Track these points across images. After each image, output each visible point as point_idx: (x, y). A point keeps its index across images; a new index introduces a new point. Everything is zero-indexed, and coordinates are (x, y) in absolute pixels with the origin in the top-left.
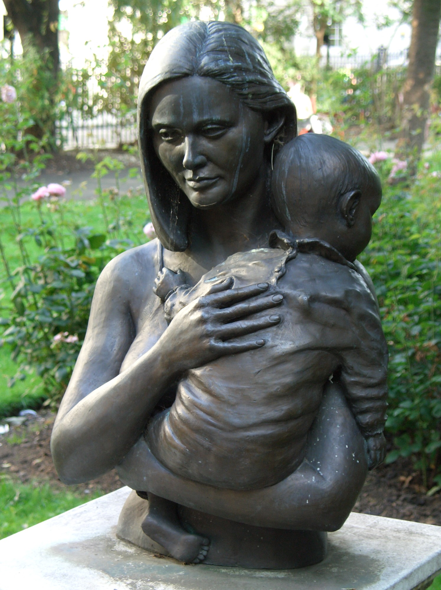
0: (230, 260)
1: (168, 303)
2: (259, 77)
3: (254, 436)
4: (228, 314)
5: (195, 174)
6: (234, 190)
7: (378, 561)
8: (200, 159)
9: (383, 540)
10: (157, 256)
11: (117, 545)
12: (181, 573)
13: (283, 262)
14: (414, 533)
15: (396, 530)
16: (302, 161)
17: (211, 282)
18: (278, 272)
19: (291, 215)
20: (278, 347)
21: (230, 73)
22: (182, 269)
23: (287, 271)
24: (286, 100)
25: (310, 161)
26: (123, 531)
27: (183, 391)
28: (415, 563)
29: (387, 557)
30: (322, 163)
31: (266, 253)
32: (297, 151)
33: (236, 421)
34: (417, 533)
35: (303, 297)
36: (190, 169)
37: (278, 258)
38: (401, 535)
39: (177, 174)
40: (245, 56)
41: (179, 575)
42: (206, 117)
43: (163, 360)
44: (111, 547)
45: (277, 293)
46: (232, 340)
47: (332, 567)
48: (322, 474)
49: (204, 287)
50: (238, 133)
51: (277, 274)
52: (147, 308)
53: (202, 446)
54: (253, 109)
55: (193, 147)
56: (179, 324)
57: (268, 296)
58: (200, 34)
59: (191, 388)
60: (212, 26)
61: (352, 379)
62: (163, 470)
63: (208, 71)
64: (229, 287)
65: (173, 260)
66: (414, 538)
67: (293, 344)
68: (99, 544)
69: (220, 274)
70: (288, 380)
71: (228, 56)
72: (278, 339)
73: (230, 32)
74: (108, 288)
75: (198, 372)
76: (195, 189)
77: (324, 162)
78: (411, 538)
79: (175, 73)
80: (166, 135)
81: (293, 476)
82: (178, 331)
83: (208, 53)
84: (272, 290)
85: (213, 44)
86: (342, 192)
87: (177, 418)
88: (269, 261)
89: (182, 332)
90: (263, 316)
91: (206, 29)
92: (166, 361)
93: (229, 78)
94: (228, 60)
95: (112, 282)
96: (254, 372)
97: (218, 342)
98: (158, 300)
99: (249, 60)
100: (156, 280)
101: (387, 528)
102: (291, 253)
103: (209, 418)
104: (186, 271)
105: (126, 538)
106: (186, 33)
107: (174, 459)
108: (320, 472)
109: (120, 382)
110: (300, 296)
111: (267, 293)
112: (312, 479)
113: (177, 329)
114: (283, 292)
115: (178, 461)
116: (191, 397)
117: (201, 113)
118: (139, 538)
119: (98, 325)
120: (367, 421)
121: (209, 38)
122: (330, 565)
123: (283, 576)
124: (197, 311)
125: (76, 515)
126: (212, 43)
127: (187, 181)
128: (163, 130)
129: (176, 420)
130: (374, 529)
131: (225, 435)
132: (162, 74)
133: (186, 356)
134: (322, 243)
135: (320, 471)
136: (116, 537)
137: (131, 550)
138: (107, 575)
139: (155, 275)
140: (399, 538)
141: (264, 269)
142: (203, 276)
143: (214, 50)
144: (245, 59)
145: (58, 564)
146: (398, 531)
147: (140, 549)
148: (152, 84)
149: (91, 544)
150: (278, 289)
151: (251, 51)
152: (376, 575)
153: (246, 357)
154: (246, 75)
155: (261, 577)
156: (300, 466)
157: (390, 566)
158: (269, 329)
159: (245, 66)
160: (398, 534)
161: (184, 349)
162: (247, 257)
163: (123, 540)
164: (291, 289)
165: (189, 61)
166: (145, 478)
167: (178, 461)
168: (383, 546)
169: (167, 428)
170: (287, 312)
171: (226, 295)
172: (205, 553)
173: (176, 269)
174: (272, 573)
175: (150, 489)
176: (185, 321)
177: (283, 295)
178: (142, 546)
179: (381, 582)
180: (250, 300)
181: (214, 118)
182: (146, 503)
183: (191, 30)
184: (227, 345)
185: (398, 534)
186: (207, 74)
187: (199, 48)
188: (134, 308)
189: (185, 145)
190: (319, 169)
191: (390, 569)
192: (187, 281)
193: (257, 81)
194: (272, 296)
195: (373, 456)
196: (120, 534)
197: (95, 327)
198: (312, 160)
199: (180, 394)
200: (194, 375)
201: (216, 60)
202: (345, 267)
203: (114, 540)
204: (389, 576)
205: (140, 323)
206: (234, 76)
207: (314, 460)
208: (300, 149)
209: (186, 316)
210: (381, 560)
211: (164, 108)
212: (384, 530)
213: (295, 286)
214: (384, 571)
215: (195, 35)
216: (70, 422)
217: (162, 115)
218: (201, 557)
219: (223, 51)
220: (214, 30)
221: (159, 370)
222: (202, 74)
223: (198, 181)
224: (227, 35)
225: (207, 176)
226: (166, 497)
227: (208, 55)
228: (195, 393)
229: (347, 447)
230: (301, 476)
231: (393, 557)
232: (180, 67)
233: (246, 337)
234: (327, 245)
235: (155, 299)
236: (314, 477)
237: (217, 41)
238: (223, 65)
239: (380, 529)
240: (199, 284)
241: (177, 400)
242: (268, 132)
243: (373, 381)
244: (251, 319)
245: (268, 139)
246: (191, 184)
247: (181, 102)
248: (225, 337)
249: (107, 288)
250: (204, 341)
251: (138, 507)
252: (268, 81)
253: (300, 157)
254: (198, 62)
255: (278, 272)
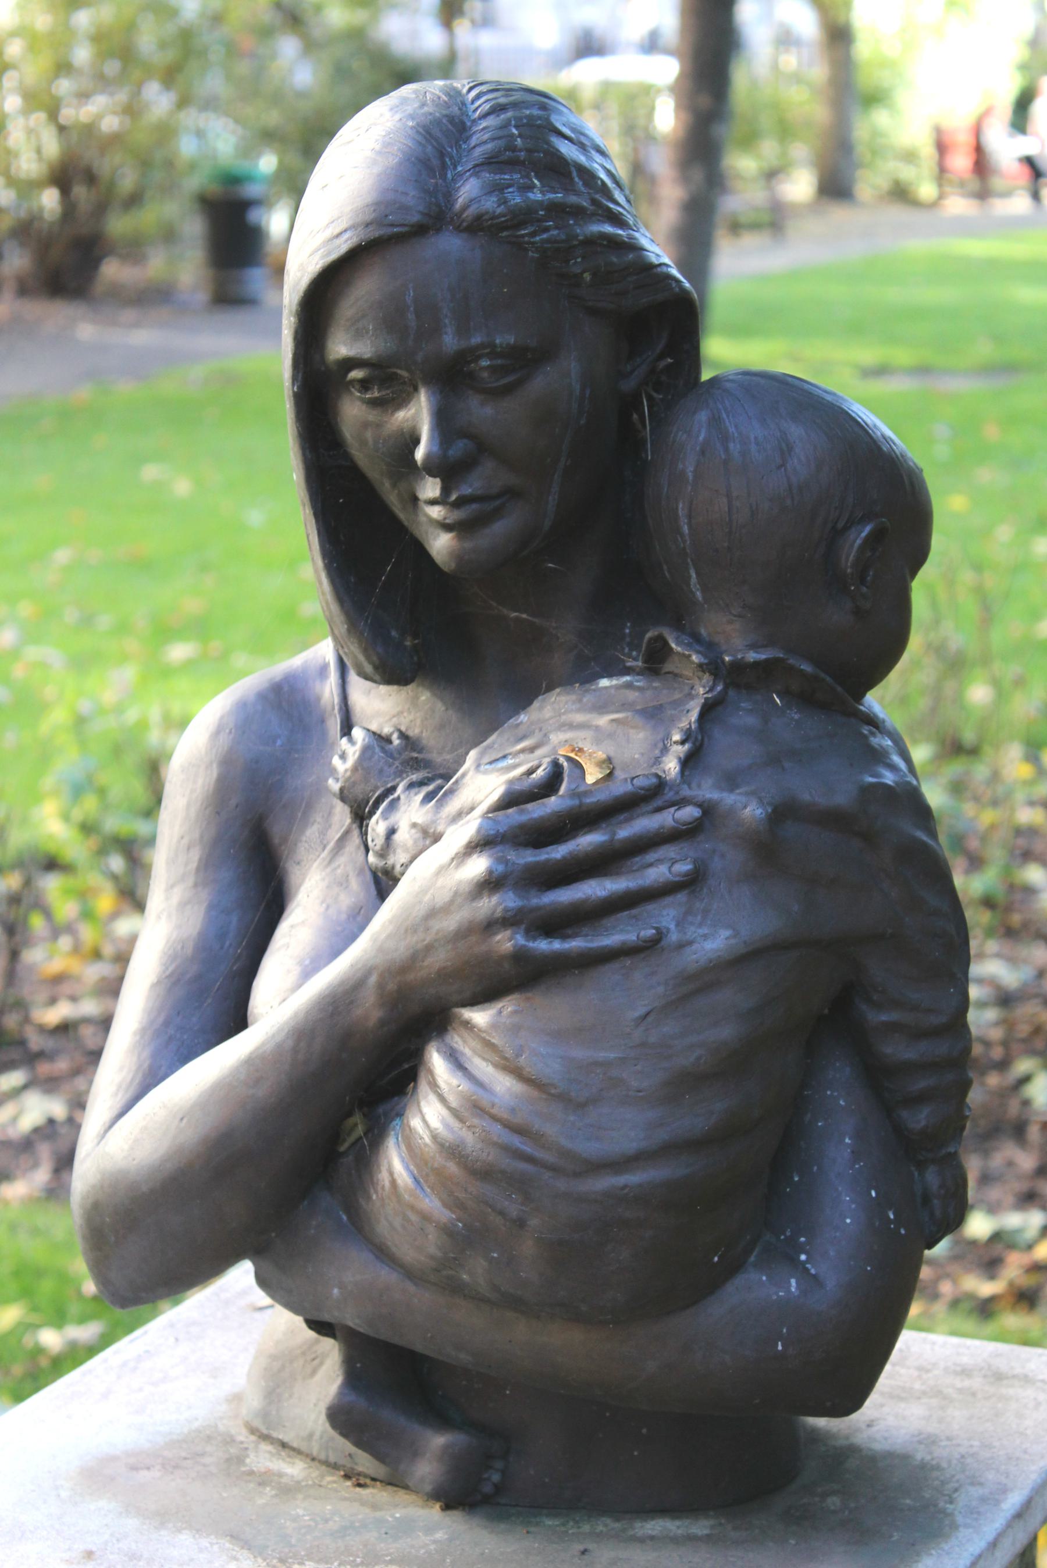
0: (541, 708)
1: (377, 826)
2: (608, 229)
3: (640, 1185)
4: (557, 862)
5: (446, 490)
6: (547, 524)
7: (938, 1468)
8: (459, 448)
9: (934, 1402)
10: (329, 690)
11: (252, 1455)
12: (439, 1535)
13: (694, 716)
14: (1007, 1378)
15: (959, 1369)
16: (731, 445)
17: (498, 770)
18: (683, 742)
19: (705, 590)
20: (694, 947)
21: (539, 220)
22: (403, 729)
23: (706, 740)
24: (674, 285)
25: (753, 448)
26: (264, 1415)
27: (437, 1061)
28: (1033, 1468)
29: (957, 1456)
30: (786, 449)
31: (639, 689)
32: (715, 421)
33: (590, 1148)
34: (1014, 1377)
35: (751, 811)
36: (434, 476)
37: (677, 704)
38: (976, 1383)
39: (394, 485)
40: (570, 173)
41: (435, 1542)
42: (476, 340)
43: (381, 986)
44: (240, 1460)
45: (681, 803)
46: (570, 932)
47: (824, 1496)
48: (813, 1271)
49: (482, 784)
50: (564, 377)
51: (679, 747)
52: (312, 832)
53: (501, 1213)
54: (593, 312)
55: (442, 419)
56: (424, 891)
57: (659, 810)
58: (451, 119)
59: (462, 1060)
60: (478, 97)
61: (884, 1018)
62: (386, 1276)
63: (479, 218)
64: (551, 784)
65: (381, 707)
66: (1011, 1391)
67: (734, 937)
68: (203, 1454)
69: (519, 747)
70: (726, 1032)
71: (528, 177)
72: (692, 923)
73: (528, 112)
74: (204, 781)
75: (480, 1017)
76: (447, 527)
77: (790, 449)
78: (1004, 1391)
79: (392, 225)
80: (364, 385)
81: (739, 1281)
82: (421, 910)
83: (477, 168)
84: (669, 795)
85: (489, 146)
86: (840, 525)
87: (427, 1140)
88: (654, 714)
89: (433, 913)
90: (651, 865)
91: (464, 104)
92: (391, 986)
93: (533, 234)
94: (531, 187)
95: (215, 766)
96: (637, 1014)
97: (534, 939)
98: (342, 815)
99: (579, 184)
100: (336, 761)
101: (934, 1365)
102: (711, 690)
103: (516, 1141)
104: (414, 732)
105: (275, 1434)
106: (412, 117)
107: (418, 1247)
108: (808, 1266)
109: (263, 1044)
110: (745, 807)
111: (658, 802)
112: (790, 1285)
113: (420, 902)
114: (700, 799)
115: (432, 1250)
116: (465, 1086)
117: (463, 330)
118: (311, 1436)
119: (183, 878)
120: (923, 1123)
121: (475, 129)
122: (819, 1490)
123: (706, 1532)
124: (475, 856)
125: (124, 1364)
126: (485, 142)
127: (422, 504)
128: (356, 374)
129: (426, 1145)
130: (903, 1371)
131: (562, 1184)
132: (352, 227)
133: (445, 975)
134: (791, 661)
135: (807, 1261)
136: (244, 1431)
137: (295, 1469)
138: (245, 1552)
139: (325, 747)
140: (974, 1394)
141: (641, 735)
142: (473, 754)
143: (492, 162)
144: (572, 179)
145: (100, 1520)
146: (965, 1372)
147: (316, 1463)
148: (329, 253)
149: (184, 1454)
150: (686, 792)
151: (582, 159)
152: (943, 1512)
153: (610, 974)
154: (575, 224)
155: (652, 1538)
156: (755, 1254)
157: (973, 1484)
158: (668, 900)
159: (573, 199)
160: (967, 1383)
161: (440, 959)
162: (588, 698)
163: (265, 1438)
164: (722, 790)
165: (427, 191)
166: (336, 1291)
167: (432, 1250)
168: (941, 1421)
169: (395, 1164)
170: (714, 851)
171: (548, 810)
172: (496, 1477)
173: (386, 730)
174: (678, 1523)
175: (351, 1318)
176: (440, 882)
177: (699, 805)
178: (323, 1457)
179: (963, 1533)
180: (614, 820)
181: (498, 341)
182: (331, 1350)
183: (426, 109)
184: (557, 945)
185: (967, 1383)
186: (475, 226)
187: (451, 158)
188: (276, 831)
189: (418, 413)
190: (779, 468)
191: (975, 1492)
192: (434, 776)
193: (604, 236)
194: (672, 810)
195: (938, 1213)
196: (257, 1423)
197: (172, 886)
198: (757, 444)
199: (431, 1072)
200: (468, 1025)
201: (498, 189)
202: (853, 720)
203: (241, 1438)
204: (979, 1513)
205: (294, 873)
206: (547, 230)
207: (788, 1234)
208: (724, 416)
209: (441, 870)
210: (944, 1465)
211: (363, 316)
212: (928, 1371)
213: (731, 781)
214: (962, 1499)
215: (438, 122)
216: (126, 1147)
217: (358, 334)
218: (487, 1489)
219: (513, 164)
220: (487, 107)
221: (369, 1010)
222: (465, 224)
223: (457, 504)
224: (521, 119)
225: (479, 492)
226: (396, 1340)
227: (476, 174)
228: (476, 1073)
229: (873, 1194)
230: (761, 1279)
231: (973, 1455)
232: (404, 208)
233: (609, 922)
234: (806, 667)
235: (332, 807)
236: (793, 1282)
237: (499, 138)
238: (518, 200)
239: (920, 1369)
240: (464, 775)
241: (423, 1086)
242: (629, 368)
243: (936, 1020)
244: (618, 874)
245: (628, 385)
246: (436, 512)
247: (409, 300)
248: (554, 924)
249: (200, 782)
250: (499, 937)
251: (304, 1353)
252: (631, 237)
253: (725, 439)
254: (449, 195)
255: (683, 742)
